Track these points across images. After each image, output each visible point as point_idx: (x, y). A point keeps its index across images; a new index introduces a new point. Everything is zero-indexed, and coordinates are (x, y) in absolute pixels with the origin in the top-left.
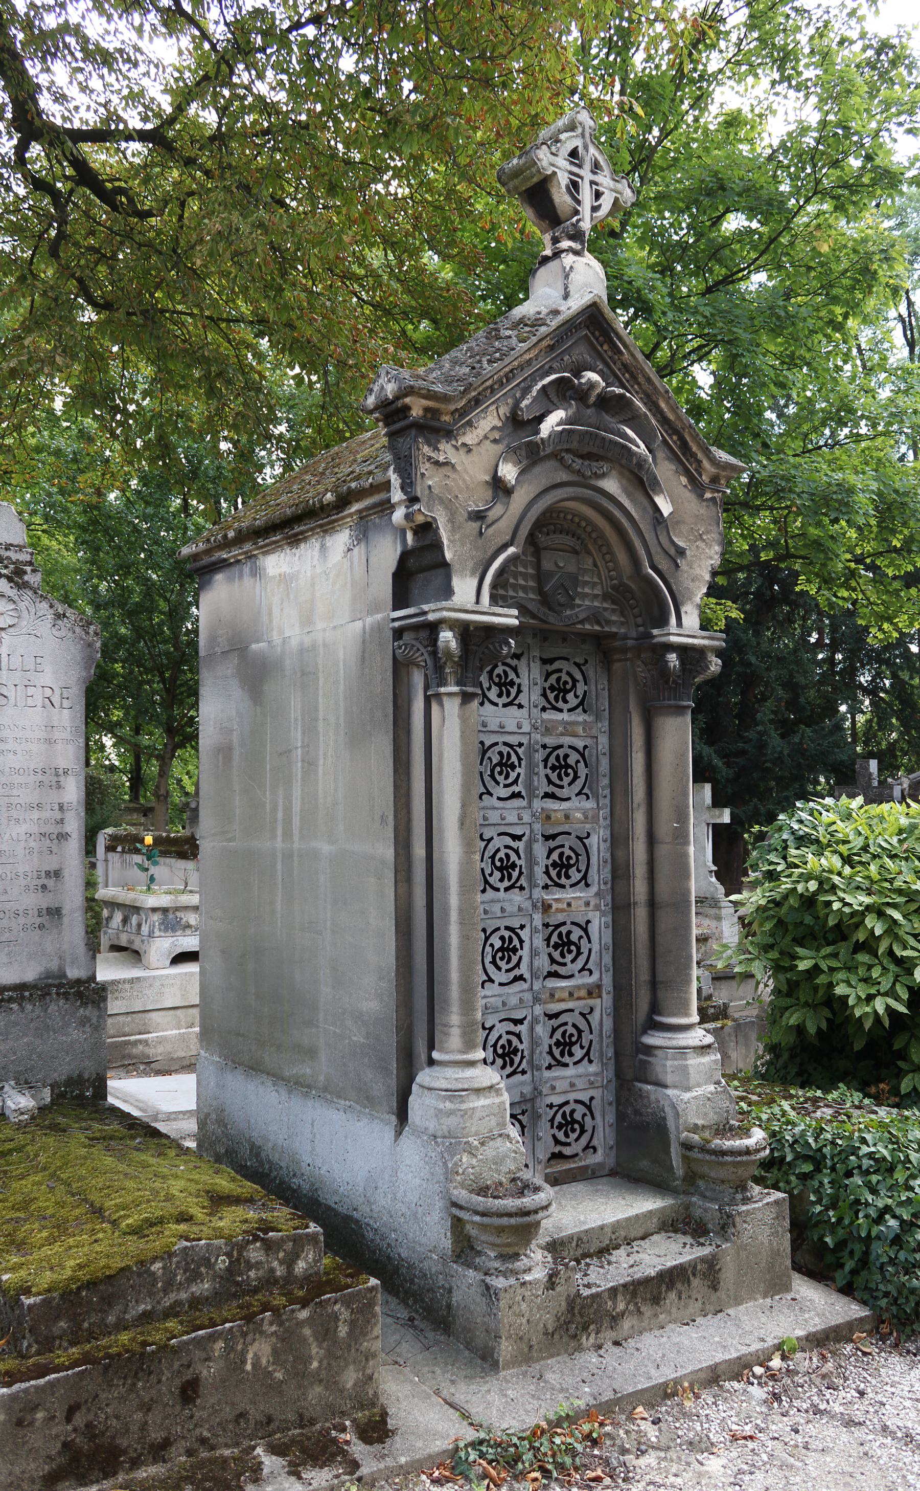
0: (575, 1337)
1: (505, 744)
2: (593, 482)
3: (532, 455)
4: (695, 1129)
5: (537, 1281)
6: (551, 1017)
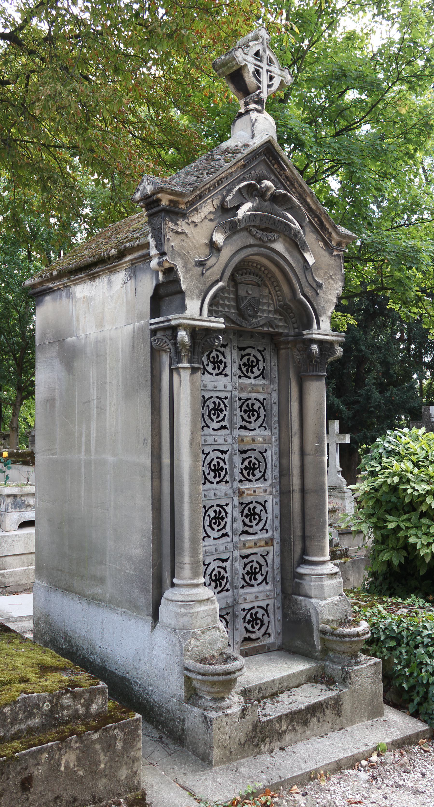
0: (257, 745)
1: (217, 397)
2: (268, 245)
3: (233, 229)
4: (328, 622)
5: (235, 714)
6: (244, 557)
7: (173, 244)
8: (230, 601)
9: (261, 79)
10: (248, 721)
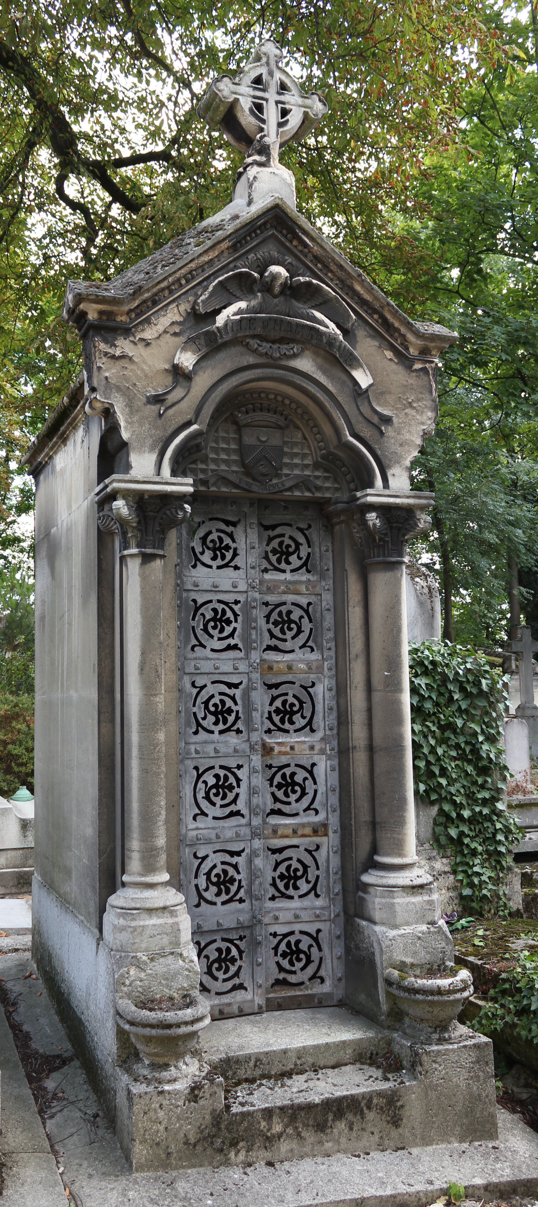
0: (221, 1150)
1: (219, 601)
2: (284, 363)
3: (212, 345)
4: (402, 967)
5: (177, 1092)
6: (274, 851)
7: (107, 374)
8: (244, 918)
9: (265, 117)
10: (203, 1107)
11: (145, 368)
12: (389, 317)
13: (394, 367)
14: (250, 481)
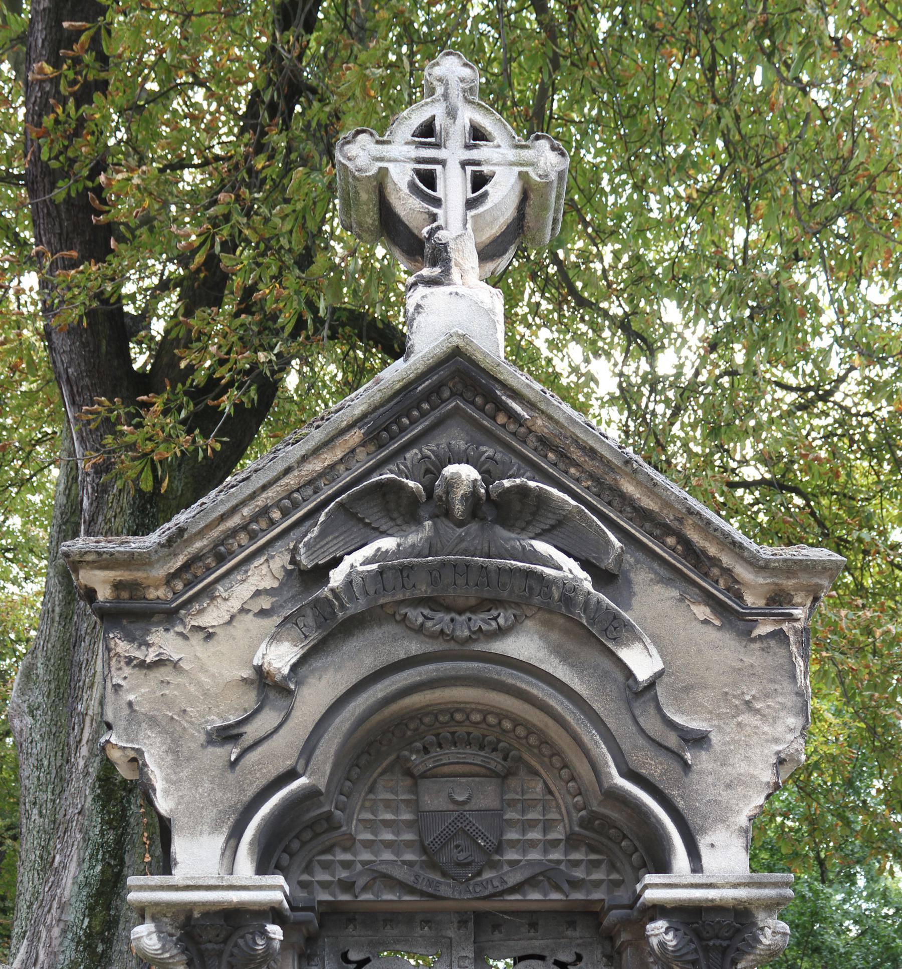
2: (481, 647)
7: (131, 697)
9: (439, 194)
11: (204, 679)
12: (694, 536)
13: (712, 635)
14: (437, 877)
